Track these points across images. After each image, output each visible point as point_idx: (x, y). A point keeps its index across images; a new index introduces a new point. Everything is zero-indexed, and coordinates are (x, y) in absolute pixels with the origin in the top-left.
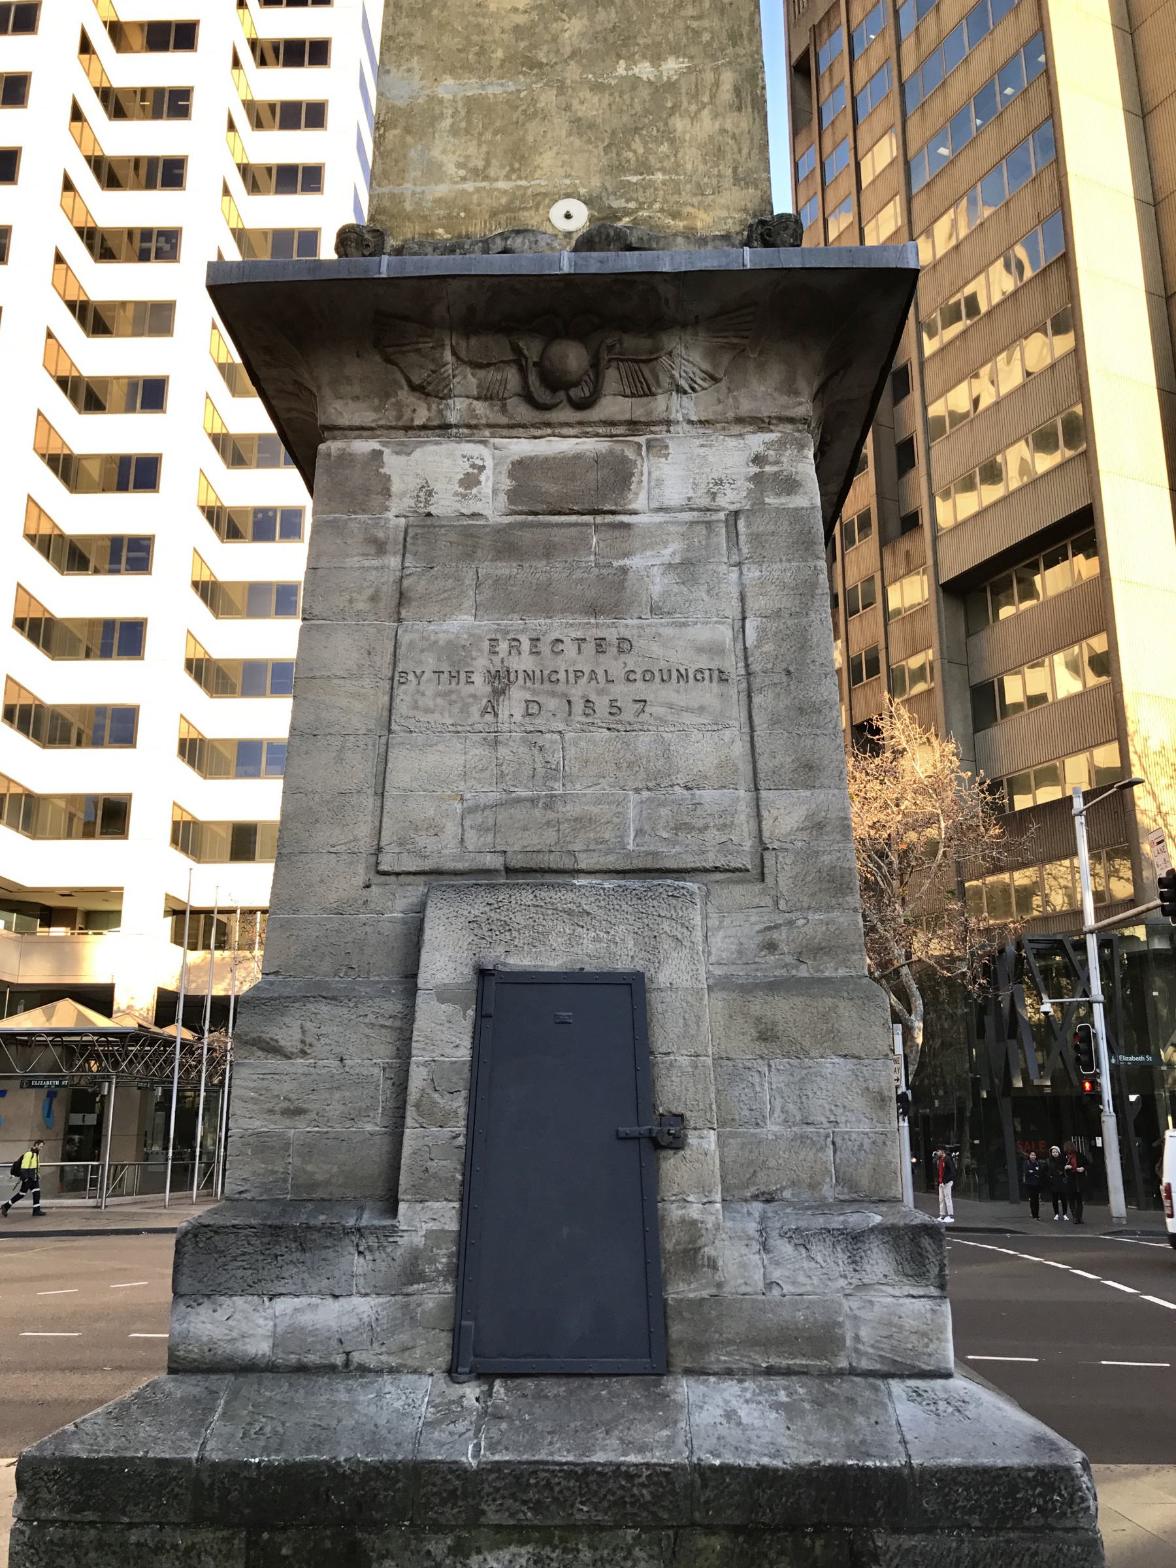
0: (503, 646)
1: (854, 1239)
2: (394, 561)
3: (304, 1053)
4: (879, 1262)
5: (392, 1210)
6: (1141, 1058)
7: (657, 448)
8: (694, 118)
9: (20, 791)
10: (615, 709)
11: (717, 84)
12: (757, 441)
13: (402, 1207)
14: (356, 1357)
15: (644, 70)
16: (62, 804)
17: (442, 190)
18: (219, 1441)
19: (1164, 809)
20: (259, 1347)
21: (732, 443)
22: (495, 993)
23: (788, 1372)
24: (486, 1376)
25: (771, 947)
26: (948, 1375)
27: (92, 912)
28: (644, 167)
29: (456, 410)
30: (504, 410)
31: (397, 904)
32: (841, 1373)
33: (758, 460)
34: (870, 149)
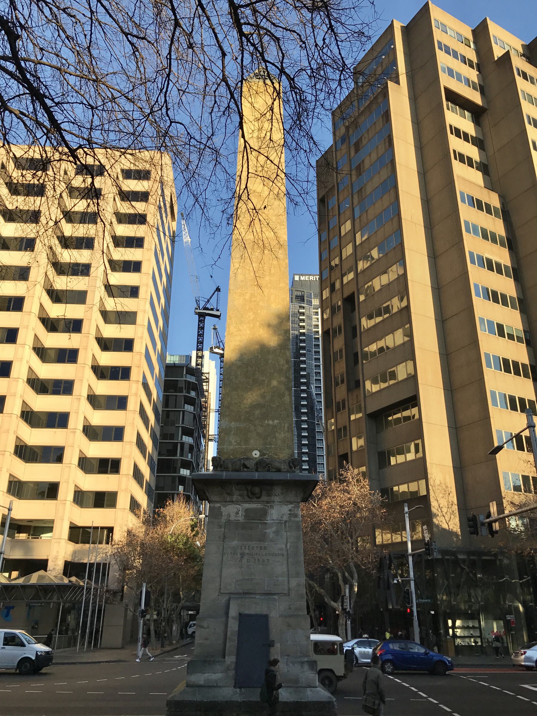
0: (243, 547)
1: (302, 663)
2: (223, 529)
3: (208, 628)
4: (306, 667)
5: (224, 657)
6: (426, 601)
7: (272, 507)
8: (280, 433)
9: (17, 480)
10: (263, 561)
11: (284, 426)
12: (290, 506)
13: (226, 657)
14: (218, 685)
15: (271, 422)
16: (32, 485)
17: (232, 447)
18: (198, 697)
19: (441, 506)
20: (202, 683)
21: (285, 506)
22: (242, 618)
23: (290, 687)
24: (240, 688)
25: (290, 608)
26: (317, 687)
27: (37, 529)
28: (270, 444)
29: (235, 498)
30: (244, 498)
31: (224, 599)
32: (299, 687)
33: (290, 510)
34: (345, 246)
